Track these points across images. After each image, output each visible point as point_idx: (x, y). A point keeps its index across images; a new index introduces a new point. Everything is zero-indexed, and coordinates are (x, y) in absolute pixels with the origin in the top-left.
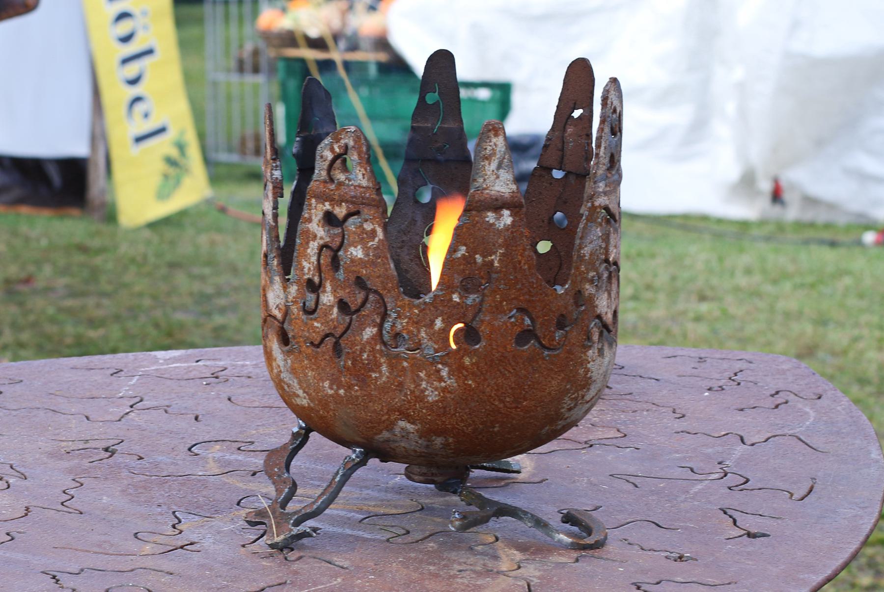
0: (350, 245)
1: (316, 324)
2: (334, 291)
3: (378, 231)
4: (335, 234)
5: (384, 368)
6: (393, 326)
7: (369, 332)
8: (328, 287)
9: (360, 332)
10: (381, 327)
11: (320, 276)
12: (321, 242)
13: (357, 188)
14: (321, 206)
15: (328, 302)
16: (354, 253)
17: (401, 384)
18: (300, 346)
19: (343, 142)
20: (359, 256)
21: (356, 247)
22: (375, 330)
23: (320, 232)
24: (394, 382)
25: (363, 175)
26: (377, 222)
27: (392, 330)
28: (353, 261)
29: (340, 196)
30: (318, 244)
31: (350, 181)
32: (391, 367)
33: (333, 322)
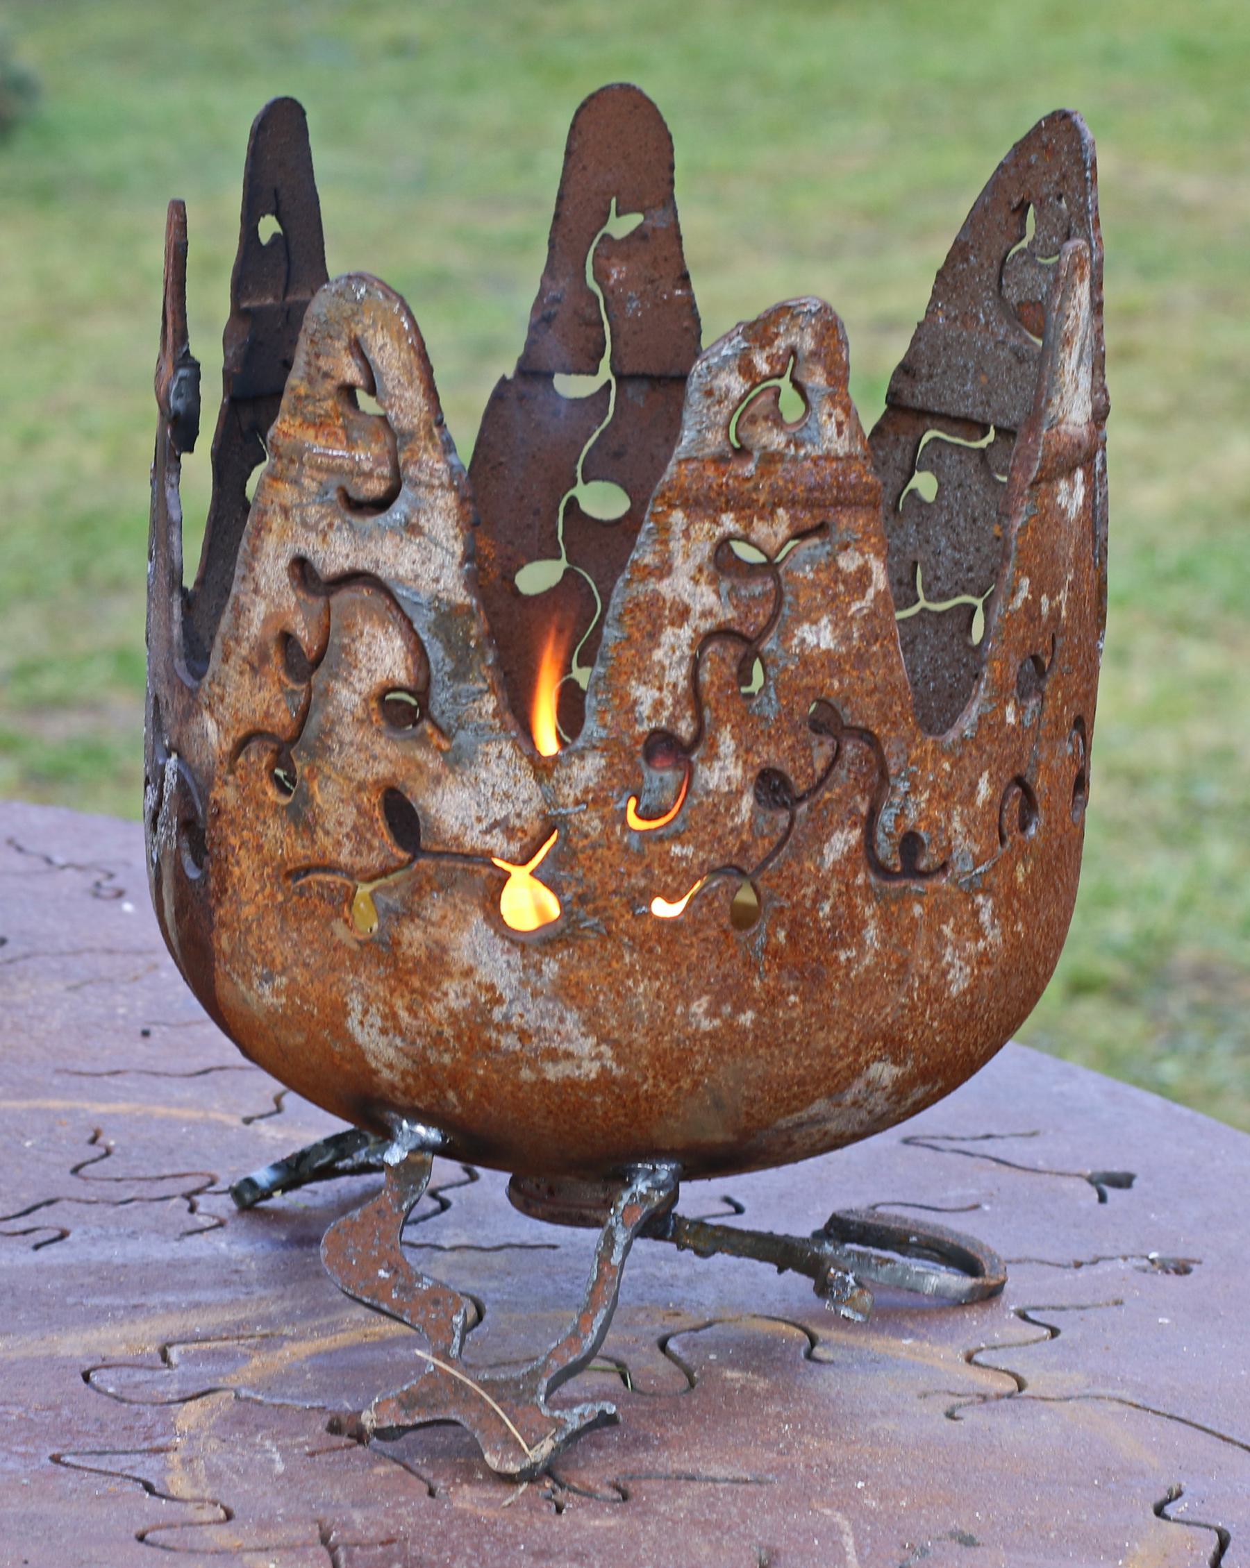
0: (799, 621)
1: (676, 850)
2: (745, 750)
3: (874, 569)
4: (753, 598)
5: (871, 933)
6: (901, 815)
7: (842, 842)
8: (727, 743)
9: (816, 847)
10: (870, 823)
11: (698, 717)
12: (706, 625)
13: (822, 463)
14: (707, 525)
15: (724, 781)
16: (811, 639)
17: (903, 965)
18: (610, 919)
19: (781, 344)
20: (823, 646)
21: (815, 622)
22: (855, 835)
23: (704, 598)
24: (889, 962)
25: (839, 425)
26: (873, 546)
27: (897, 826)
28: (805, 661)
29: (773, 490)
30: (695, 631)
31: (798, 446)
32: (887, 923)
33: (739, 834)
